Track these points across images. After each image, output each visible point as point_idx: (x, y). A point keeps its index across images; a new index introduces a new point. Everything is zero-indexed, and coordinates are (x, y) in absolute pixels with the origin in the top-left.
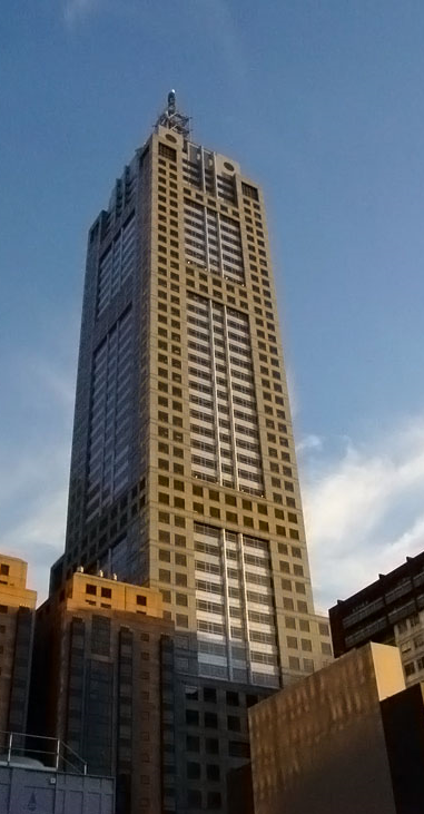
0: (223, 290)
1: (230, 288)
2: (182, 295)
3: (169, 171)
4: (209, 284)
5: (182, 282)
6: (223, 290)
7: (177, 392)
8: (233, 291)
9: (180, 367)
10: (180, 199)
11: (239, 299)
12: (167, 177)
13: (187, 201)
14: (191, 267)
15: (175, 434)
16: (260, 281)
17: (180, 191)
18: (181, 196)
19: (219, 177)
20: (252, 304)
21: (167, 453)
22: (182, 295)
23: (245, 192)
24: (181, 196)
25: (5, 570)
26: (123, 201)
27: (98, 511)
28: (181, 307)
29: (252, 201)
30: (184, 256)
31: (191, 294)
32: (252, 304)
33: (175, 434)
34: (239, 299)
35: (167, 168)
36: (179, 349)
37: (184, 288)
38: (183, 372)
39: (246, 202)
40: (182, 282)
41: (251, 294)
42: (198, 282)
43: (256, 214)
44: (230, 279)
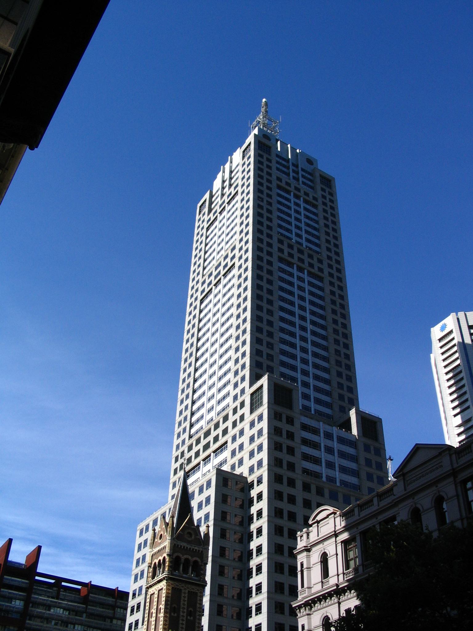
0: (305, 257)
1: (310, 256)
2: (275, 260)
3: (266, 163)
4: (295, 252)
5: (275, 250)
6: (305, 257)
7: (270, 334)
8: (313, 259)
9: (272, 315)
10: (274, 185)
11: (317, 265)
12: (265, 176)
13: (279, 187)
14: (282, 238)
15: (268, 355)
16: (332, 244)
17: (274, 178)
18: (275, 183)
19: (303, 170)
20: (326, 270)
21: (262, 345)
22: (275, 260)
23: (322, 182)
24: (275, 183)
25: (28, 2)
26: (227, 183)
27: (202, 423)
28: (275, 268)
29: (327, 190)
30: (276, 229)
31: (281, 260)
32: (326, 270)
33: (268, 355)
34: (317, 265)
35: (264, 160)
36: (272, 345)
37: (276, 254)
38: (274, 288)
39: (323, 190)
40: (275, 250)
41: (326, 262)
42: (286, 250)
43: (327, 213)
44: (310, 249)
